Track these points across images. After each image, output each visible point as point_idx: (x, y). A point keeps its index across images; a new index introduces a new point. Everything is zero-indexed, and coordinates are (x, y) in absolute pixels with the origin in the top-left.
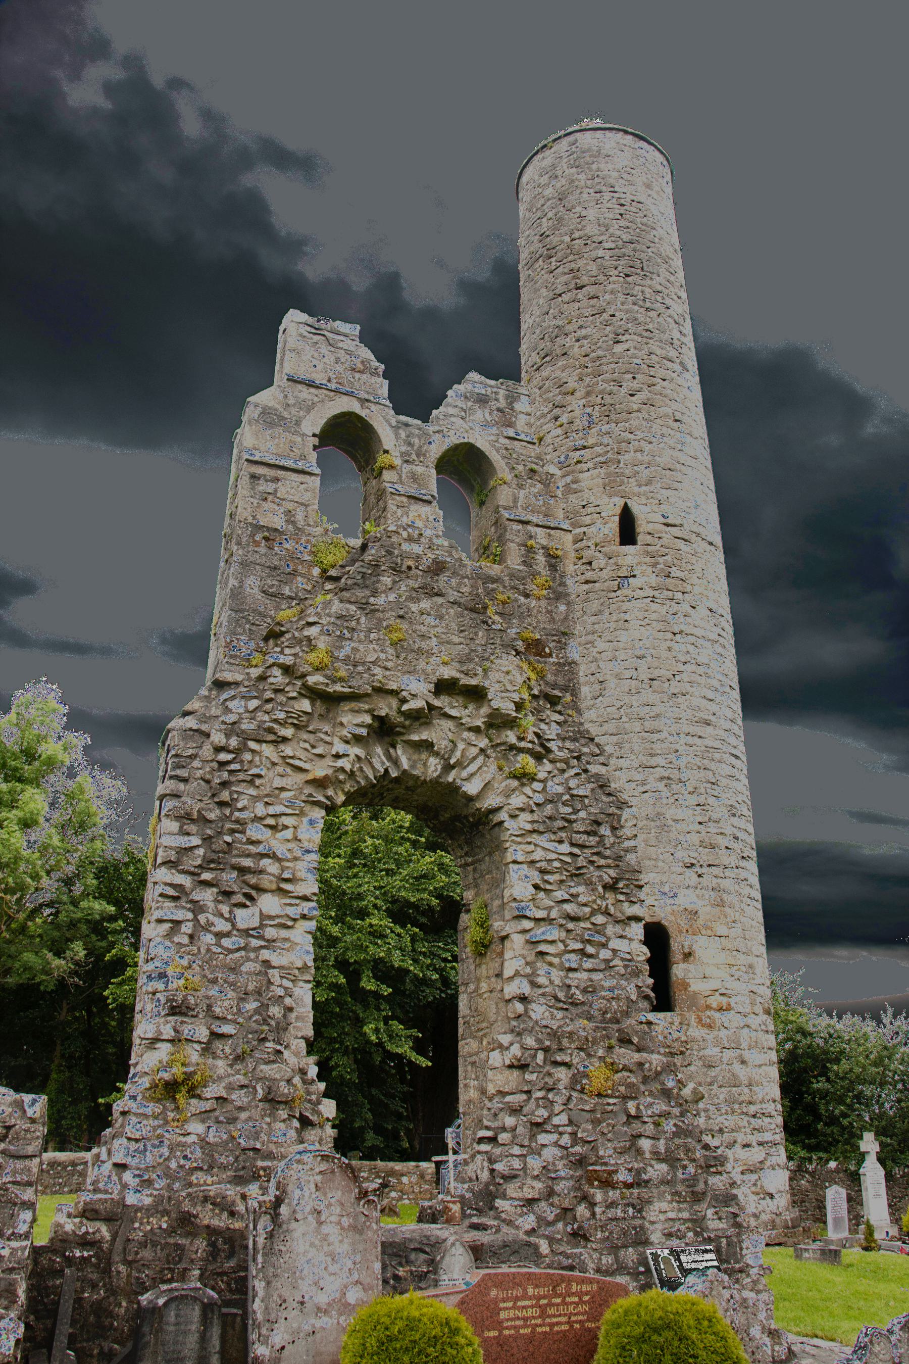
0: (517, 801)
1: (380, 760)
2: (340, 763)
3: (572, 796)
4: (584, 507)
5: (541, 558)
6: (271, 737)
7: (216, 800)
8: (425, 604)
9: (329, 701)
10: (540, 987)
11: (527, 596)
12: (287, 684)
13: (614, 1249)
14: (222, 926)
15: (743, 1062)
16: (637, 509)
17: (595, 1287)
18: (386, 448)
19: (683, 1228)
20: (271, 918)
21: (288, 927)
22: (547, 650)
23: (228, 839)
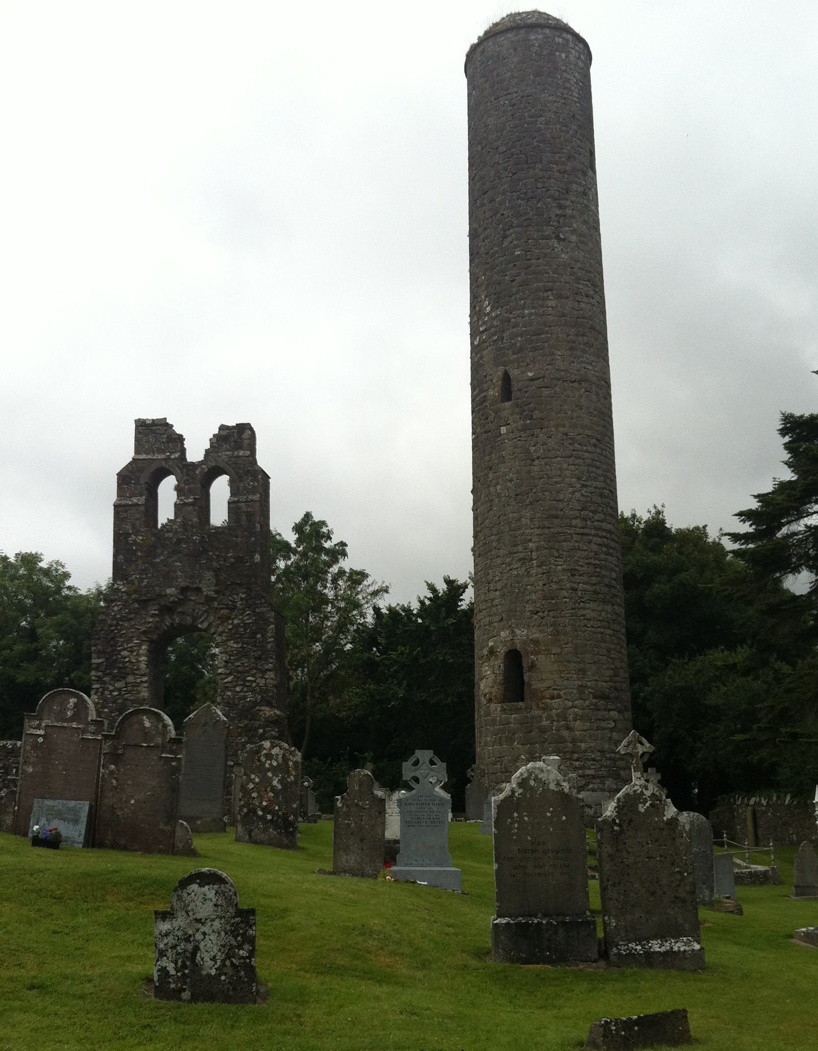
0: (220, 629)
1: (168, 622)
5: (244, 518)
8: (174, 558)
9: (144, 603)
11: (236, 537)
14: (111, 688)
15: (568, 728)
16: (514, 373)
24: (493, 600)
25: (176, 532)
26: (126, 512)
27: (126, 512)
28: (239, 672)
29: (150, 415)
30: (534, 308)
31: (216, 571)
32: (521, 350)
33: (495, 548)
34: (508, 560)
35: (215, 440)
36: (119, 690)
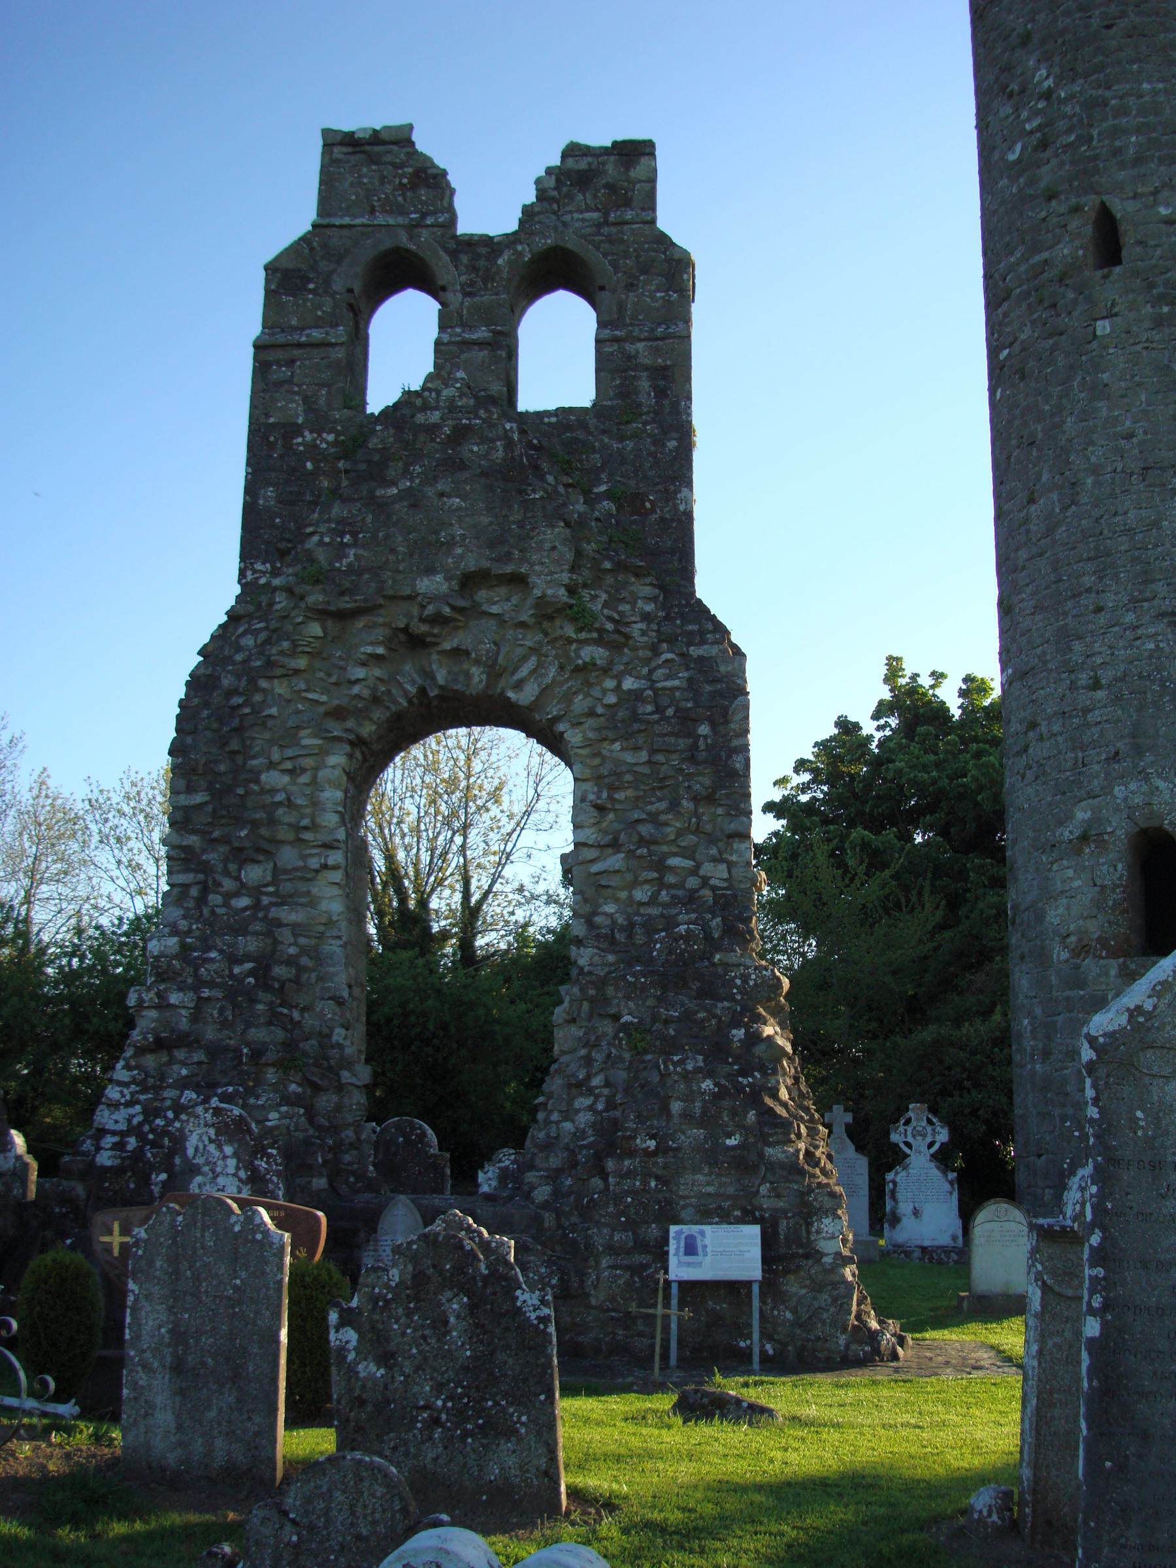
0: (580, 703)
2: (356, 690)
3: (656, 691)
4: (1044, 219)
5: (645, 384)
6: (279, 672)
7: (227, 749)
10: (598, 927)
12: (293, 608)
13: (631, 1225)
16: (1119, 207)
17: (282, 1214)
18: (441, 283)
19: (726, 1204)
20: (286, 872)
21: (310, 880)
22: (648, 505)
23: (240, 791)
24: (1086, 711)
25: (452, 408)
26: (291, 362)
27: (291, 362)
28: (642, 841)
29: (357, 119)
30: (1162, 80)
31: (576, 527)
32: (1138, 161)
33: (1089, 591)
34: (1130, 618)
35: (551, 182)
36: (256, 892)
